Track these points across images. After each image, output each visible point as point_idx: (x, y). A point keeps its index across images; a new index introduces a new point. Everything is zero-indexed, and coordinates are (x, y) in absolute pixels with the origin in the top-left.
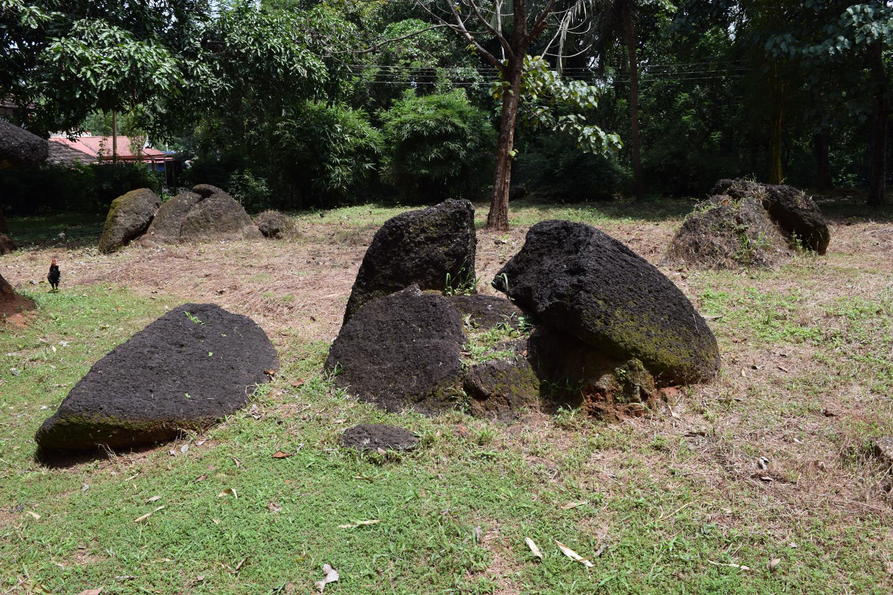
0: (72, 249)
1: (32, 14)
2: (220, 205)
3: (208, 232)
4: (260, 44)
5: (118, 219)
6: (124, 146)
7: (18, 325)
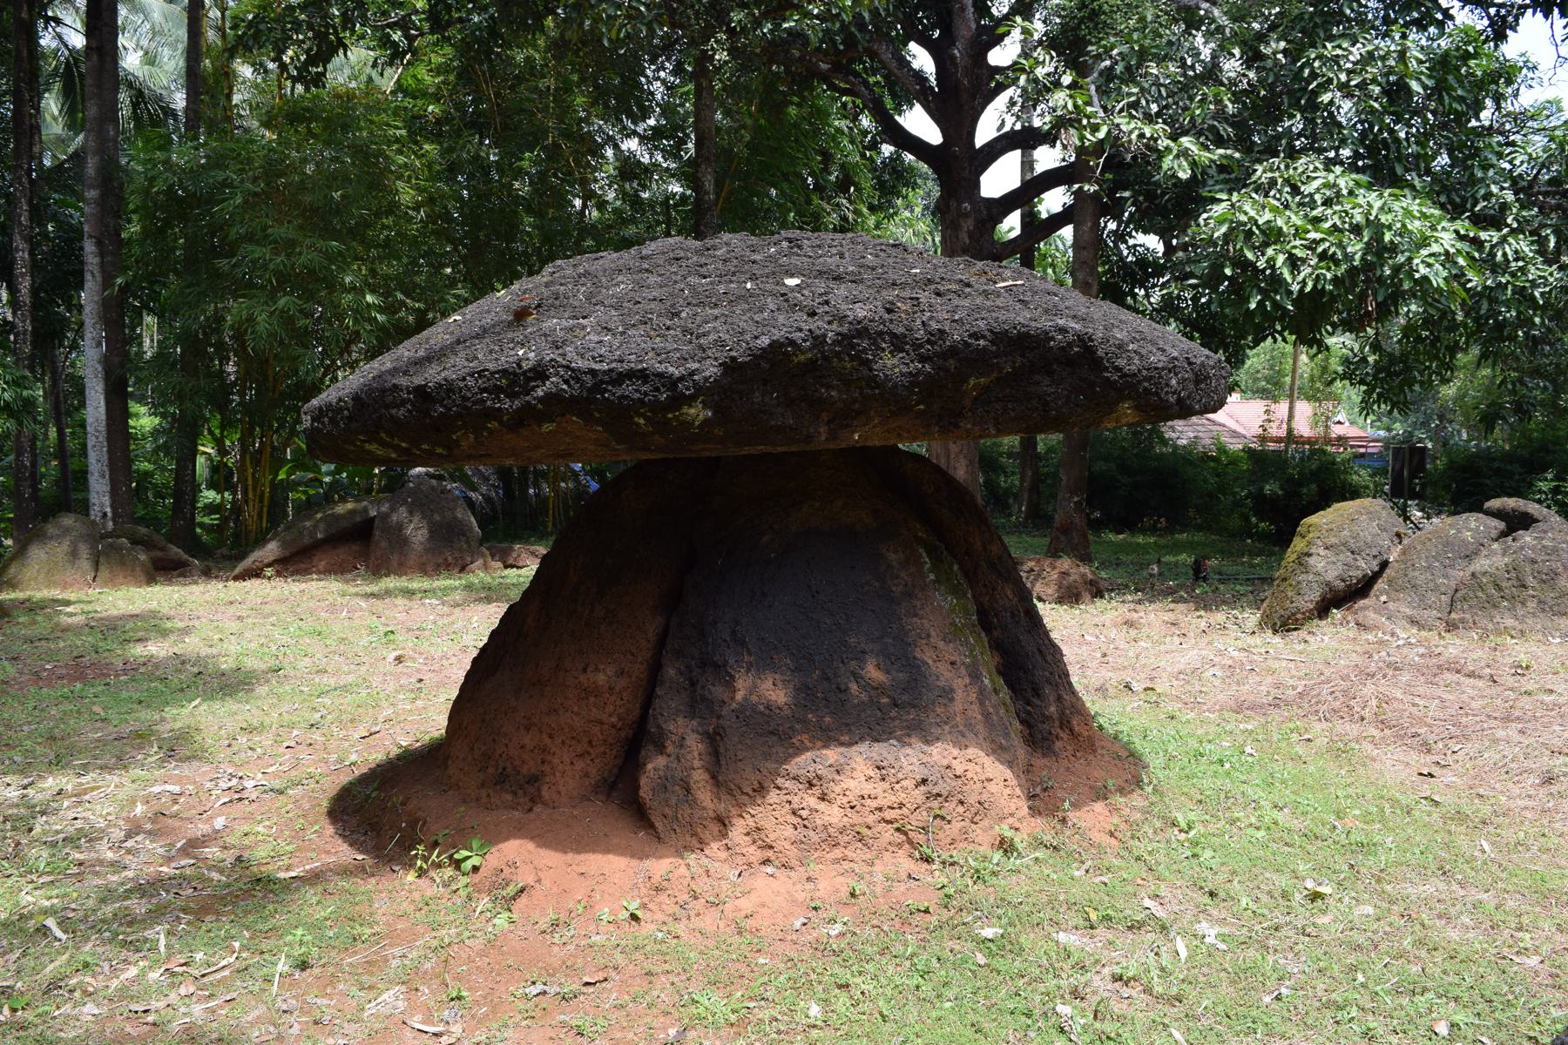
0: (1206, 608)
1: (1184, 153)
2: (1555, 550)
3: (1520, 612)
5: (1312, 561)
6: (1304, 419)
7: (1097, 837)
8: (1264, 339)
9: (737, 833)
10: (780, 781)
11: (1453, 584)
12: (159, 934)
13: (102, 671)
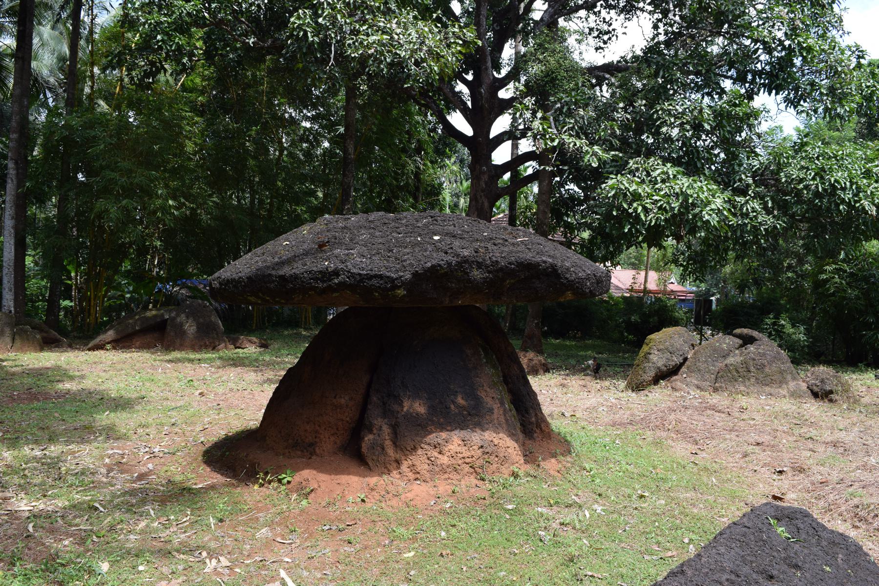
1: (595, 154)
2: (764, 354)
3: (747, 383)
4: (822, 178)
5: (651, 357)
6: (653, 280)
7: (552, 472)
8: (632, 246)
9: (404, 467)
10: (422, 445)
11: (717, 369)
12: (150, 509)
13: (47, 397)
